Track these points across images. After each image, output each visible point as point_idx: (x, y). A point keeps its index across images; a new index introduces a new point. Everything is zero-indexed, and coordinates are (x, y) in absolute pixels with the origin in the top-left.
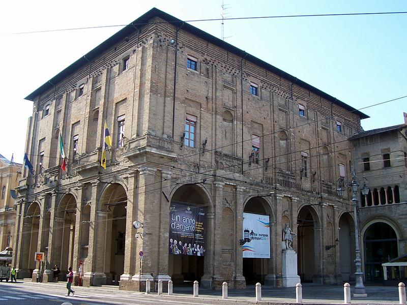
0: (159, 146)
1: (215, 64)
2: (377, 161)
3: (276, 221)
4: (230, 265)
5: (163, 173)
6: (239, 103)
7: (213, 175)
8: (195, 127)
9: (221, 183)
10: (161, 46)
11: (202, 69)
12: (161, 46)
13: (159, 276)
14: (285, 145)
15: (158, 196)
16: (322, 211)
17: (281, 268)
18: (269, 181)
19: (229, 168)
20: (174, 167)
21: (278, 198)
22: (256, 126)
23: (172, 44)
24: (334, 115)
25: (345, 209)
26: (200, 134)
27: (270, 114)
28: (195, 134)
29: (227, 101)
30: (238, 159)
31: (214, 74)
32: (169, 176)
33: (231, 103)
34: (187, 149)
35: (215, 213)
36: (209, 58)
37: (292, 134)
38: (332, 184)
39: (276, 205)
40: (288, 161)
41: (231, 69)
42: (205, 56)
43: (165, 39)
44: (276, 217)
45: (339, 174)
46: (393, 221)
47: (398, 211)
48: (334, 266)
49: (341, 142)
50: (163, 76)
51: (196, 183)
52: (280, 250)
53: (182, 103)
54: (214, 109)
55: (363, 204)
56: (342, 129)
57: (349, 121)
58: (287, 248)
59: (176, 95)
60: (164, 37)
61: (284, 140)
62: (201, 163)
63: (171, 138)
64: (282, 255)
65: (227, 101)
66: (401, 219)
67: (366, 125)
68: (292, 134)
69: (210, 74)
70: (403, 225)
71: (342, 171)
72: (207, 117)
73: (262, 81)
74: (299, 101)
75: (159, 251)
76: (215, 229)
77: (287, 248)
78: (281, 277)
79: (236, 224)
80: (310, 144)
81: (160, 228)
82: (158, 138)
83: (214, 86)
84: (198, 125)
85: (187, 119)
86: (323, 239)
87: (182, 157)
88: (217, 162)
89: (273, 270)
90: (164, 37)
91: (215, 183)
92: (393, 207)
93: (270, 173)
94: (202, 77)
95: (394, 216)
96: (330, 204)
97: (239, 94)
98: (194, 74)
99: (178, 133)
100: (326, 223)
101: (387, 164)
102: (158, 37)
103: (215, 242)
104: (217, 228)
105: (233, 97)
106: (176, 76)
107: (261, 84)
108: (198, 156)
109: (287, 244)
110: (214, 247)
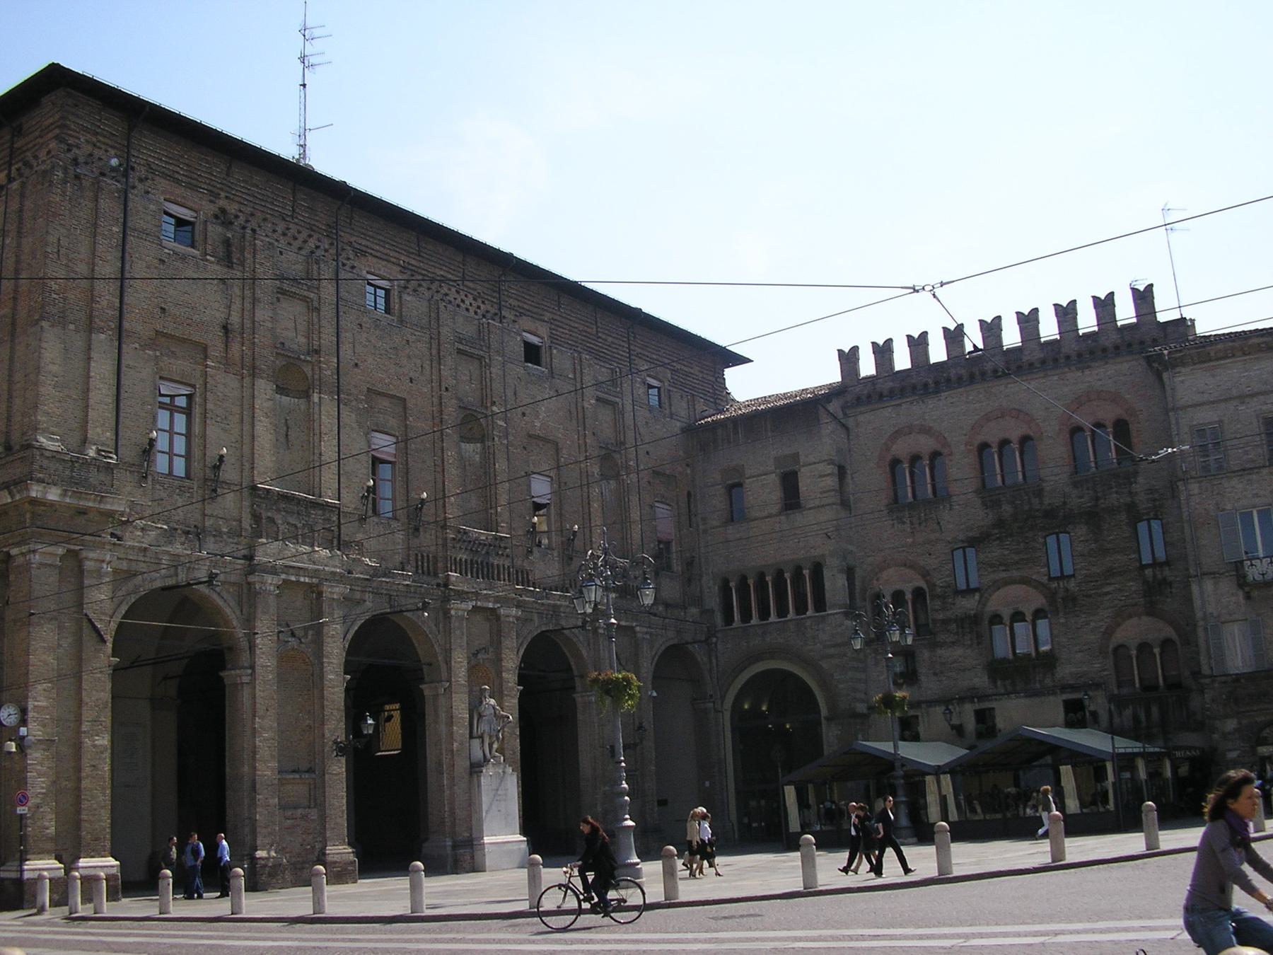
2: (763, 492)
6: (328, 338)
12: (77, 177)
14: (477, 458)
17: (470, 816)
22: (385, 403)
23: (113, 169)
24: (637, 361)
27: (427, 367)
28: (188, 435)
29: (291, 334)
33: (303, 340)
36: (232, 208)
37: (501, 423)
39: (448, 632)
41: (304, 234)
43: (91, 155)
44: (449, 669)
53: (144, 347)
54: (247, 360)
55: (729, 619)
59: (126, 325)
60: (88, 149)
65: (291, 334)
67: (743, 386)
68: (501, 423)
72: (226, 385)
79: (322, 697)
80: (557, 450)
83: (248, 293)
88: (256, 518)
90: (88, 149)
93: (428, 540)
97: (327, 312)
103: (254, 753)
105: (310, 323)
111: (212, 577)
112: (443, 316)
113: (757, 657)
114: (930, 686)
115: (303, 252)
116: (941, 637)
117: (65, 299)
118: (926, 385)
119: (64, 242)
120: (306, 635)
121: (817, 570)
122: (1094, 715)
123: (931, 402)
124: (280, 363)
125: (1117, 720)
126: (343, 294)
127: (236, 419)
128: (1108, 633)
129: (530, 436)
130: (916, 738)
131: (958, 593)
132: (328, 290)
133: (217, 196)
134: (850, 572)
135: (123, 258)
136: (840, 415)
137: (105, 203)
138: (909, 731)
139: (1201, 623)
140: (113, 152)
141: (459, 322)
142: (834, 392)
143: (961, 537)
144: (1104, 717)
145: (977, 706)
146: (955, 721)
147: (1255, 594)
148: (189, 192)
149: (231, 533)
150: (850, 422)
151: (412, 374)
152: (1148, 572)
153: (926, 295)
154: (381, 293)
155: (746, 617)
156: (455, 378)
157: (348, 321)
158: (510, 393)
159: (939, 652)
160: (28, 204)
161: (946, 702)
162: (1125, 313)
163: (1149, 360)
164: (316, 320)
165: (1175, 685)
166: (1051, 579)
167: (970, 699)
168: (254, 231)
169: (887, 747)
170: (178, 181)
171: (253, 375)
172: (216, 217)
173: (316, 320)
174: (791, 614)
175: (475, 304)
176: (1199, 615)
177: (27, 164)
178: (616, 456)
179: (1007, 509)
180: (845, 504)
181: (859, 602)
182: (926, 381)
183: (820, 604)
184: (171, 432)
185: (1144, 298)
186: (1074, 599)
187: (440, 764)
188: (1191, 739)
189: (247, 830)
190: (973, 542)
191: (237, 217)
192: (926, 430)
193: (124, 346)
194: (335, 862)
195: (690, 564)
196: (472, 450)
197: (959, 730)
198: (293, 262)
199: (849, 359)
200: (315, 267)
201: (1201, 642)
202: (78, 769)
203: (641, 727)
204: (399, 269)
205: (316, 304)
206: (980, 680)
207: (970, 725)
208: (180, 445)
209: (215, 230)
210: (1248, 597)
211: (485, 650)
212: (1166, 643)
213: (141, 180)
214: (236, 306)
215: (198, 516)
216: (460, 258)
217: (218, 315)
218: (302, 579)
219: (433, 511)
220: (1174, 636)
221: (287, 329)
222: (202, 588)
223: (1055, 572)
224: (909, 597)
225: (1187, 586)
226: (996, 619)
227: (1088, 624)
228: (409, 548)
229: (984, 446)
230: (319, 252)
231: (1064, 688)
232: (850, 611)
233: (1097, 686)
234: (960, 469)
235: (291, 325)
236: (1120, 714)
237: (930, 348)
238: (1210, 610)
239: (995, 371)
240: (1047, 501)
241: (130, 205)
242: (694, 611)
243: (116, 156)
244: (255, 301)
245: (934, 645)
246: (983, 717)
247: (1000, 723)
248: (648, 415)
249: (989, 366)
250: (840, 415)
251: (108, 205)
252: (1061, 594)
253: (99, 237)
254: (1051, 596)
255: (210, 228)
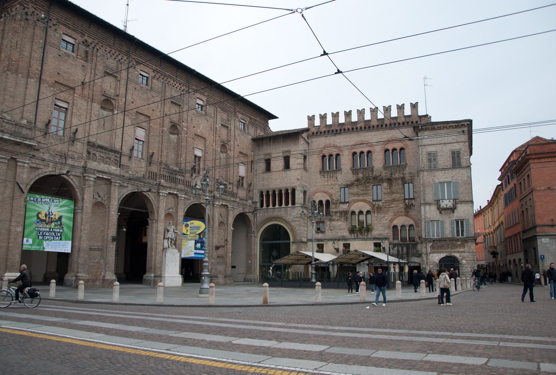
0: (15, 132)
1: (98, 47)
3: (158, 218)
4: (98, 263)
5: (19, 161)
6: (122, 91)
7: (83, 167)
8: (66, 114)
9: (92, 176)
10: (27, 19)
11: (79, 51)
12: (27, 19)
13: (7, 274)
14: (175, 140)
15: (10, 185)
16: (213, 210)
17: (161, 267)
18: (153, 176)
19: (103, 160)
20: (33, 156)
21: (161, 194)
22: (142, 117)
23: (42, 19)
24: (238, 113)
25: (241, 209)
26: (71, 121)
27: (160, 107)
28: (65, 121)
29: (108, 88)
30: (116, 152)
31: (94, 58)
32: (26, 165)
33: (113, 91)
34: (53, 138)
35: (82, 207)
36: (90, 40)
37: (185, 129)
38: (227, 183)
39: (159, 201)
40: (178, 155)
41: (117, 53)
42: (86, 38)
43: (33, 12)
44: (158, 214)
45: (238, 172)
46: (288, 223)
47: (293, 214)
48: (224, 266)
49: (242, 140)
50: (26, 54)
51: (59, 175)
52: (160, 248)
53: (50, 86)
54: (91, 96)
55: (262, 205)
56: (246, 128)
57: (255, 120)
58: (169, 247)
59: (43, 77)
60: (33, 10)
61: (173, 134)
62: (70, 153)
63: (31, 126)
64: (162, 254)
65: (108, 88)
66: (296, 221)
67: (274, 126)
68: (185, 129)
69: (89, 58)
70: (297, 228)
71: (242, 171)
72: (82, 104)
73: (154, 71)
74: (198, 95)
75: (8, 247)
76: (81, 225)
77: (169, 247)
78: (160, 276)
79: (108, 220)
80: (205, 141)
81: (11, 221)
82: (14, 123)
83: (93, 72)
84: (69, 112)
85: (55, 105)
86: (213, 238)
87: (46, 146)
88: (89, 153)
89: (151, 268)
90: (33, 10)
91: (85, 175)
92: (289, 209)
93: (154, 169)
94: (79, 60)
95: (289, 218)
96: (224, 203)
97: (123, 82)
98: (68, 56)
99: (42, 118)
100: (217, 222)
101: (287, 166)
102: (24, 9)
103: (81, 238)
104: (84, 223)
105: (116, 85)
106: (45, 56)
107: (153, 74)
108: (66, 145)
109: (169, 242)
110: (80, 244)
111: (68, 172)
112: (167, 89)
113: (271, 219)
114: (329, 234)
115: (117, 60)
116: (334, 218)
117: (18, 64)
118: (337, 131)
119: (19, 43)
120: (104, 197)
121: (294, 190)
122: (384, 248)
123: (338, 137)
124: (103, 98)
125: (391, 251)
126: (130, 76)
127: (84, 116)
128: (392, 221)
129: (196, 135)
130: (322, 252)
131: (341, 203)
132: (124, 74)
133: (84, 35)
134: (305, 192)
135: (44, 52)
136: (306, 138)
137: (37, 31)
138: (321, 249)
139: (423, 220)
140: (43, 13)
141: (173, 92)
142: (307, 130)
143: (344, 183)
144: (387, 249)
145: (375, 241)
146: (336, 247)
147: (443, 212)
148: (73, 32)
149: (79, 158)
150: (309, 141)
151: (154, 108)
152: (407, 201)
153: (298, 15)
154: (145, 78)
155: (268, 205)
156: (170, 111)
157: (131, 86)
158: (189, 119)
159: (333, 222)
160: (7, 28)
161: (334, 240)
162: (408, 111)
163: (414, 128)
164: (118, 84)
165: (412, 239)
166: (373, 201)
167: (342, 240)
168: (97, 49)
169: (310, 254)
170: (69, 28)
171: (92, 101)
172: (83, 43)
173: (118, 84)
174: (283, 206)
175: (180, 86)
176: (423, 217)
177: (8, 12)
178: (227, 145)
179: (360, 175)
180: (305, 169)
181: (307, 203)
182: (337, 129)
183: (294, 203)
184: (59, 119)
185: (414, 106)
186: (381, 208)
187: (152, 247)
188: (416, 260)
189: (75, 266)
190: (348, 186)
191: (91, 44)
192: (336, 147)
193: (41, 85)
194: (108, 280)
195: (250, 185)
196: (174, 137)
197: (337, 250)
198: (112, 63)
199: (311, 119)
200: (120, 65)
201: (423, 227)
202: (9, 239)
203: (226, 240)
204: (152, 70)
205: (119, 79)
206: (346, 234)
207: (341, 248)
208: (62, 124)
209: (82, 48)
210: (441, 213)
211: (172, 208)
212: (411, 226)
213: (54, 25)
214: (88, 76)
215: (66, 150)
216: (176, 70)
217: (80, 78)
218: (104, 177)
219: (157, 157)
220: (414, 224)
221: (107, 86)
222: (65, 176)
223: (375, 198)
224: (324, 203)
225: (420, 207)
226: (353, 213)
227: (384, 217)
228: (147, 170)
229: (354, 153)
230: (122, 61)
231: (375, 239)
232: (304, 206)
233: (386, 239)
234: (346, 161)
235: (108, 85)
236: (393, 249)
237: (340, 118)
238: (427, 215)
239: (361, 128)
240: (374, 174)
241: (48, 33)
242: (250, 201)
243: (44, 14)
244: (95, 74)
245: (331, 220)
246: (347, 246)
247: (352, 249)
248: (239, 132)
249: (359, 126)
250: (306, 138)
251: (39, 32)
252: (376, 206)
253: (34, 44)
254: (373, 206)
255: (80, 46)
